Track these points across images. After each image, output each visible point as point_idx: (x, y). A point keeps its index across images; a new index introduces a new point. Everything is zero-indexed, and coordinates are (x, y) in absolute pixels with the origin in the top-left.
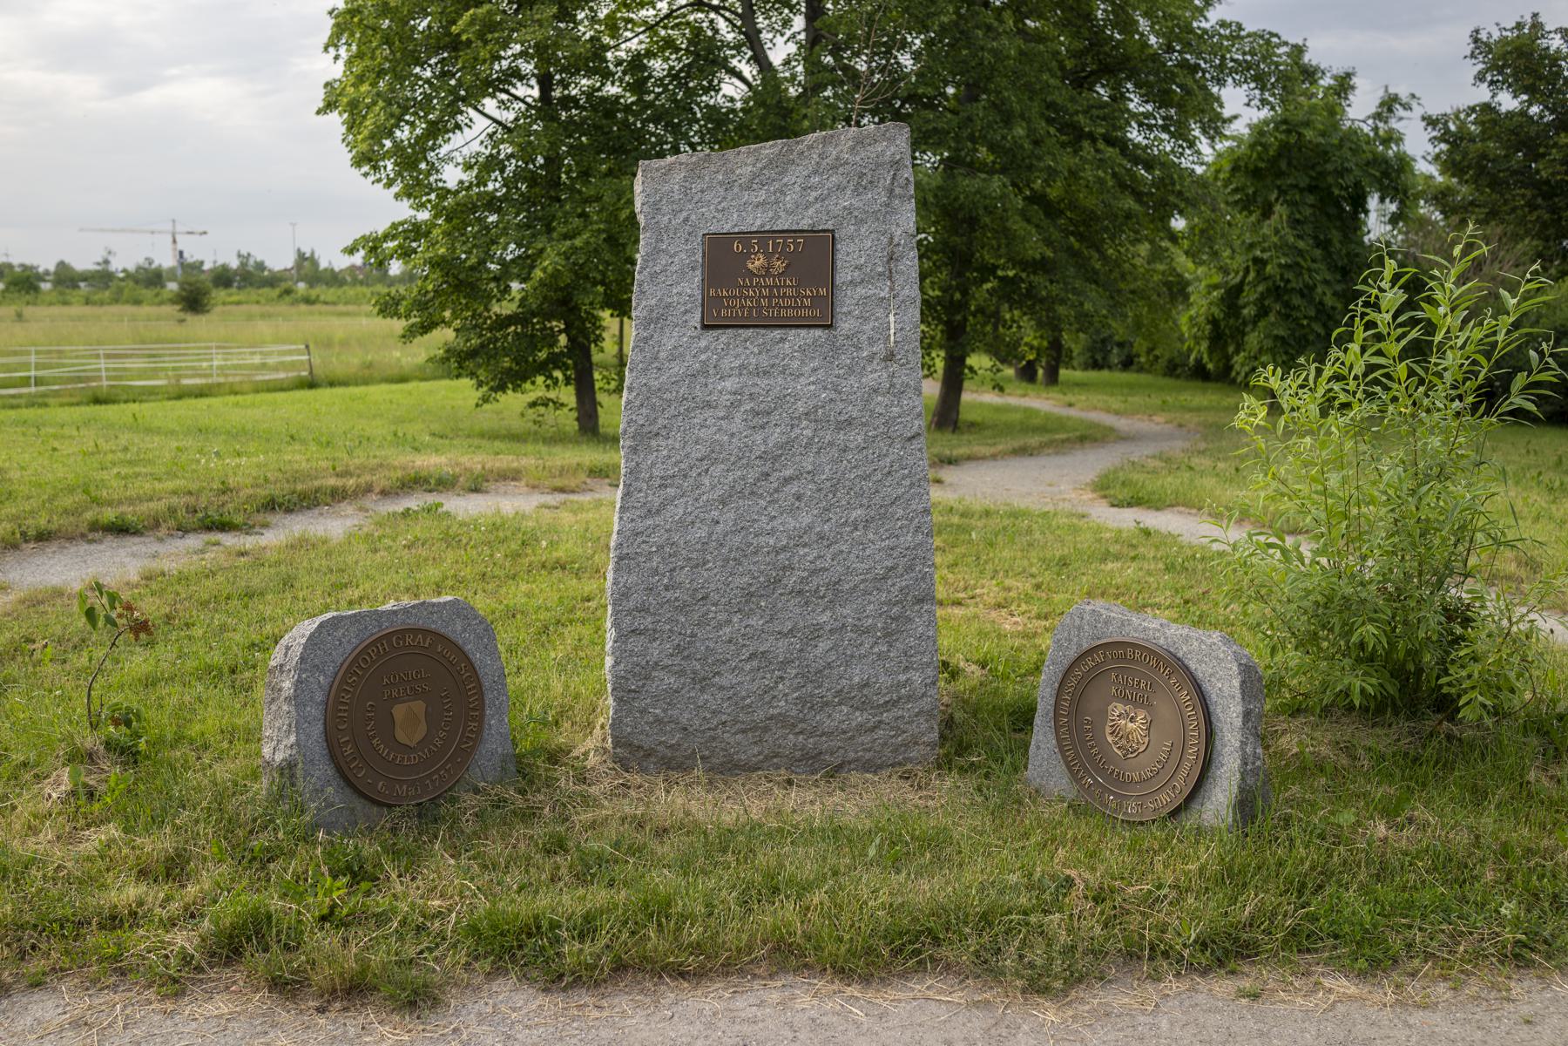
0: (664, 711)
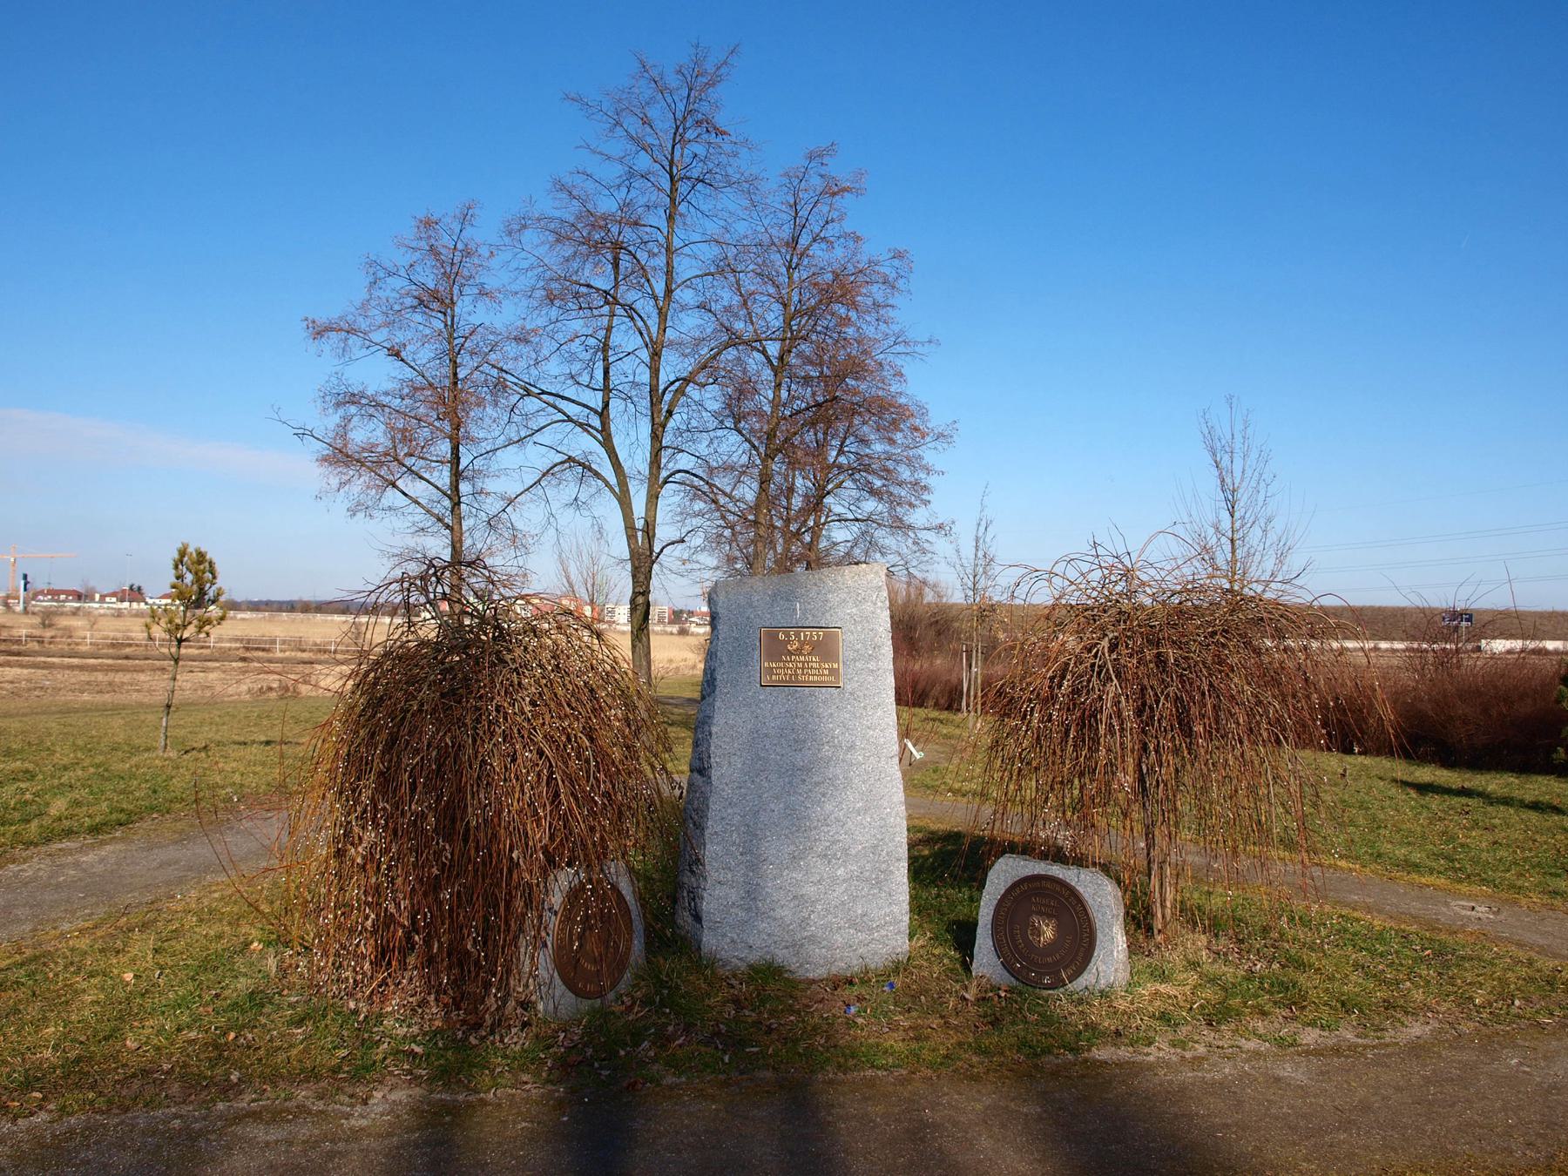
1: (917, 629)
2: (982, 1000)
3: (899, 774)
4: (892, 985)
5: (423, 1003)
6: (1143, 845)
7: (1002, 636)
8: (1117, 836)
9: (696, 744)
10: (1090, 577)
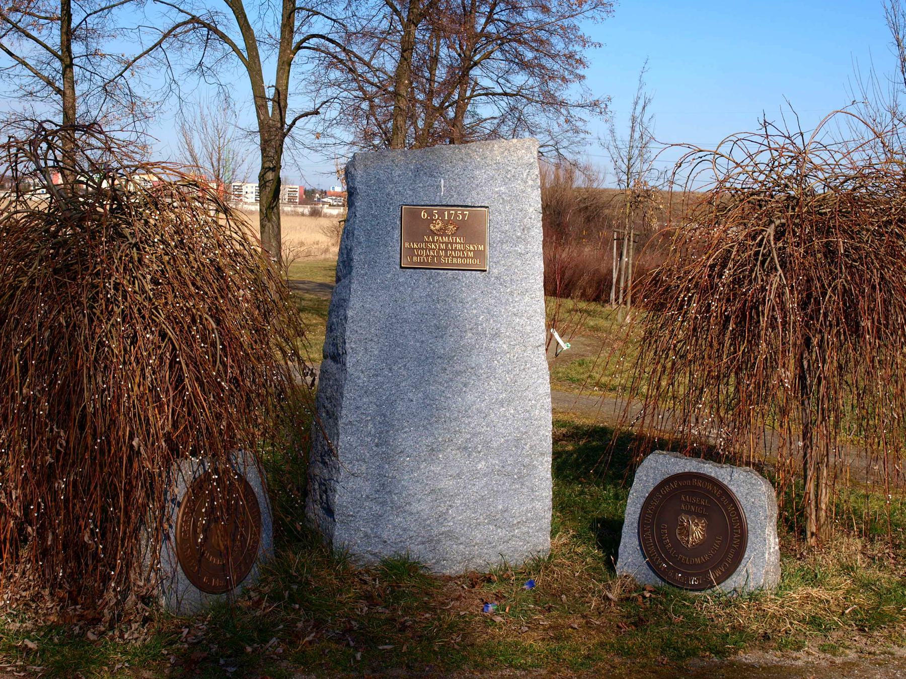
0: (372, 529)
1: (569, 216)
2: (625, 600)
3: (546, 365)
4: (531, 584)
5: (37, 597)
6: (801, 444)
7: (655, 224)
8: (771, 436)
9: (330, 329)
10: (758, 159)
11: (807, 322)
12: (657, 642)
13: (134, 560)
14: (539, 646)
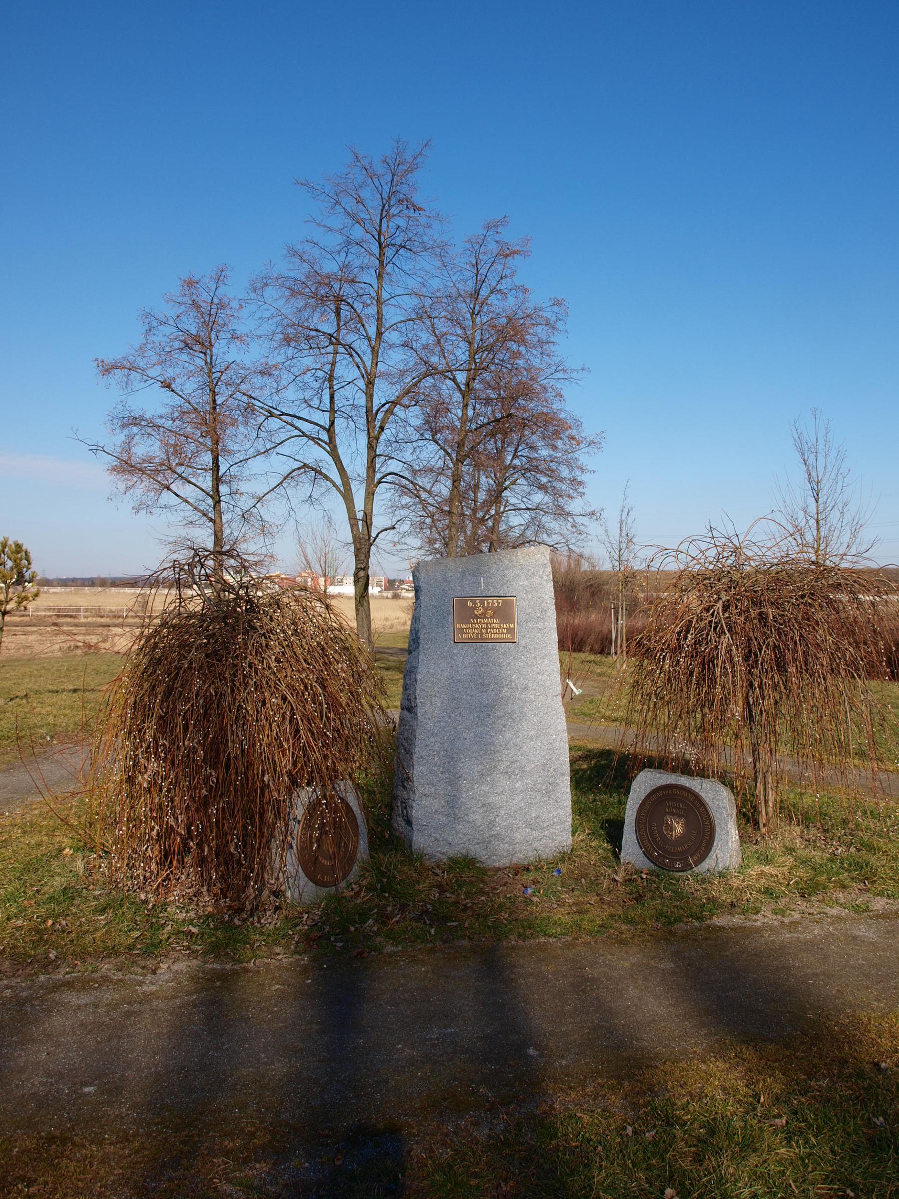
0: (440, 835)
2: (628, 881)
4: (559, 871)
5: (198, 894)
6: (750, 760)
7: (641, 595)
8: (730, 754)
11: (750, 671)
12: (653, 912)
13: (267, 864)
14: (566, 919)
